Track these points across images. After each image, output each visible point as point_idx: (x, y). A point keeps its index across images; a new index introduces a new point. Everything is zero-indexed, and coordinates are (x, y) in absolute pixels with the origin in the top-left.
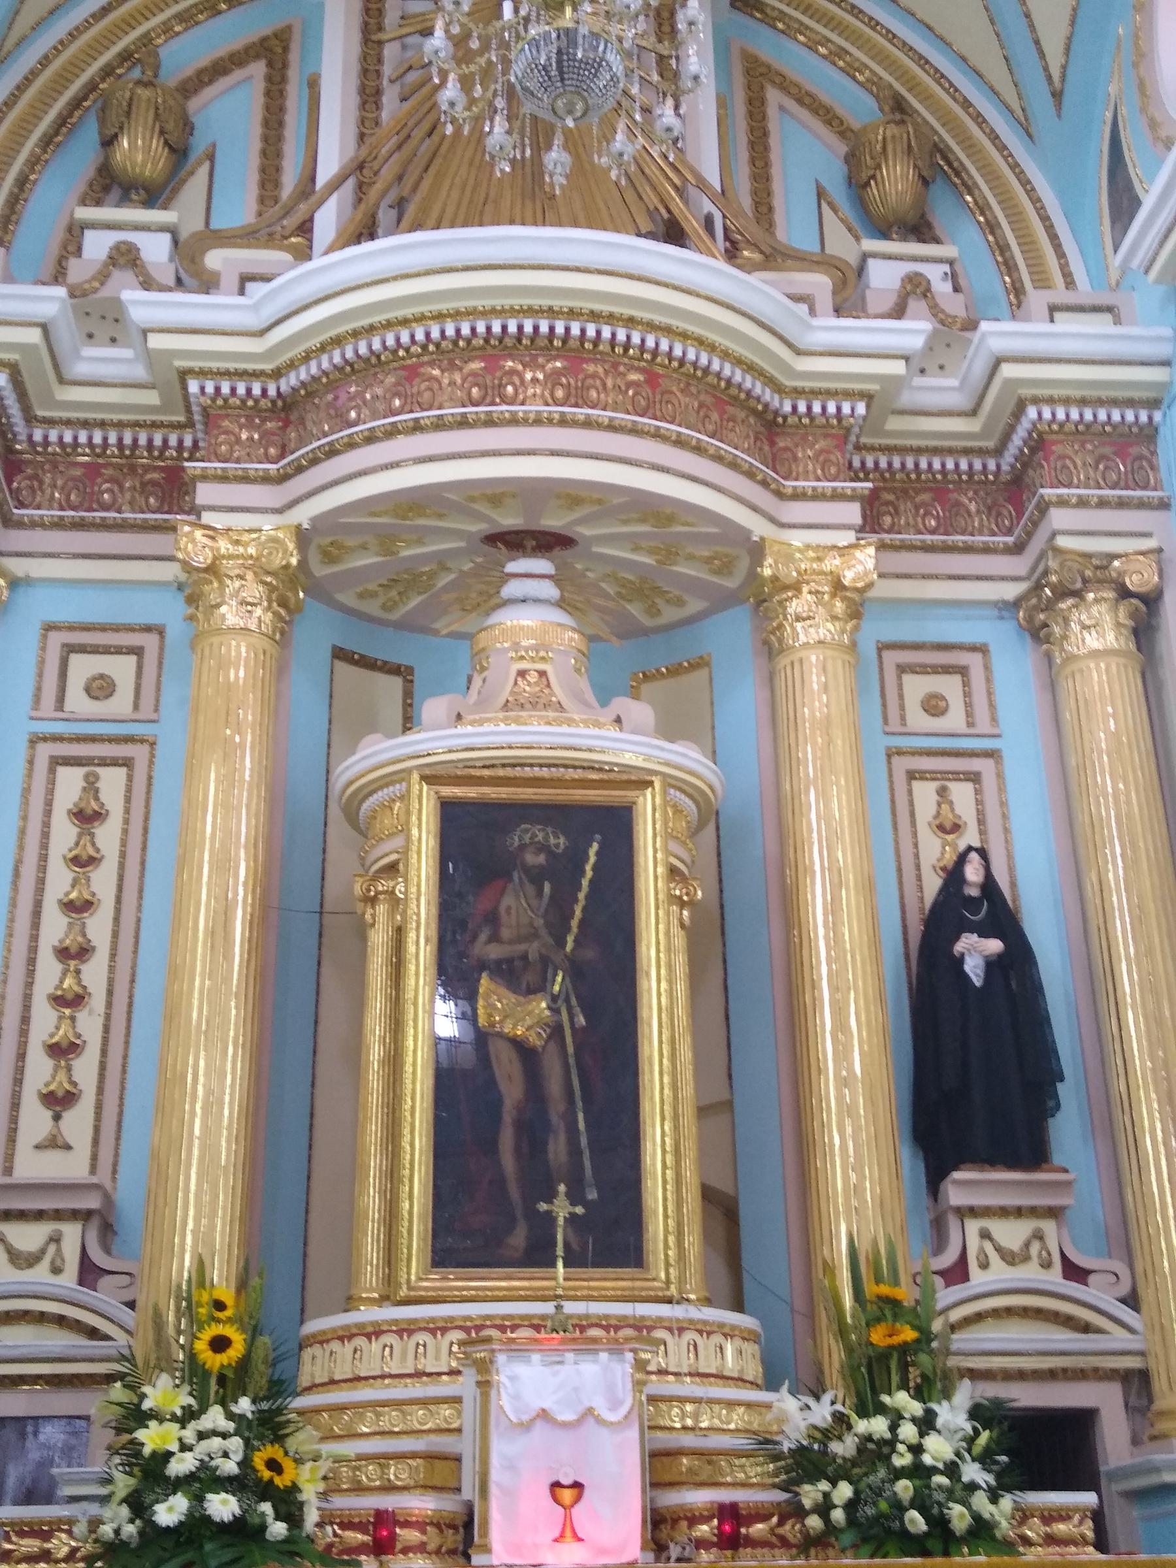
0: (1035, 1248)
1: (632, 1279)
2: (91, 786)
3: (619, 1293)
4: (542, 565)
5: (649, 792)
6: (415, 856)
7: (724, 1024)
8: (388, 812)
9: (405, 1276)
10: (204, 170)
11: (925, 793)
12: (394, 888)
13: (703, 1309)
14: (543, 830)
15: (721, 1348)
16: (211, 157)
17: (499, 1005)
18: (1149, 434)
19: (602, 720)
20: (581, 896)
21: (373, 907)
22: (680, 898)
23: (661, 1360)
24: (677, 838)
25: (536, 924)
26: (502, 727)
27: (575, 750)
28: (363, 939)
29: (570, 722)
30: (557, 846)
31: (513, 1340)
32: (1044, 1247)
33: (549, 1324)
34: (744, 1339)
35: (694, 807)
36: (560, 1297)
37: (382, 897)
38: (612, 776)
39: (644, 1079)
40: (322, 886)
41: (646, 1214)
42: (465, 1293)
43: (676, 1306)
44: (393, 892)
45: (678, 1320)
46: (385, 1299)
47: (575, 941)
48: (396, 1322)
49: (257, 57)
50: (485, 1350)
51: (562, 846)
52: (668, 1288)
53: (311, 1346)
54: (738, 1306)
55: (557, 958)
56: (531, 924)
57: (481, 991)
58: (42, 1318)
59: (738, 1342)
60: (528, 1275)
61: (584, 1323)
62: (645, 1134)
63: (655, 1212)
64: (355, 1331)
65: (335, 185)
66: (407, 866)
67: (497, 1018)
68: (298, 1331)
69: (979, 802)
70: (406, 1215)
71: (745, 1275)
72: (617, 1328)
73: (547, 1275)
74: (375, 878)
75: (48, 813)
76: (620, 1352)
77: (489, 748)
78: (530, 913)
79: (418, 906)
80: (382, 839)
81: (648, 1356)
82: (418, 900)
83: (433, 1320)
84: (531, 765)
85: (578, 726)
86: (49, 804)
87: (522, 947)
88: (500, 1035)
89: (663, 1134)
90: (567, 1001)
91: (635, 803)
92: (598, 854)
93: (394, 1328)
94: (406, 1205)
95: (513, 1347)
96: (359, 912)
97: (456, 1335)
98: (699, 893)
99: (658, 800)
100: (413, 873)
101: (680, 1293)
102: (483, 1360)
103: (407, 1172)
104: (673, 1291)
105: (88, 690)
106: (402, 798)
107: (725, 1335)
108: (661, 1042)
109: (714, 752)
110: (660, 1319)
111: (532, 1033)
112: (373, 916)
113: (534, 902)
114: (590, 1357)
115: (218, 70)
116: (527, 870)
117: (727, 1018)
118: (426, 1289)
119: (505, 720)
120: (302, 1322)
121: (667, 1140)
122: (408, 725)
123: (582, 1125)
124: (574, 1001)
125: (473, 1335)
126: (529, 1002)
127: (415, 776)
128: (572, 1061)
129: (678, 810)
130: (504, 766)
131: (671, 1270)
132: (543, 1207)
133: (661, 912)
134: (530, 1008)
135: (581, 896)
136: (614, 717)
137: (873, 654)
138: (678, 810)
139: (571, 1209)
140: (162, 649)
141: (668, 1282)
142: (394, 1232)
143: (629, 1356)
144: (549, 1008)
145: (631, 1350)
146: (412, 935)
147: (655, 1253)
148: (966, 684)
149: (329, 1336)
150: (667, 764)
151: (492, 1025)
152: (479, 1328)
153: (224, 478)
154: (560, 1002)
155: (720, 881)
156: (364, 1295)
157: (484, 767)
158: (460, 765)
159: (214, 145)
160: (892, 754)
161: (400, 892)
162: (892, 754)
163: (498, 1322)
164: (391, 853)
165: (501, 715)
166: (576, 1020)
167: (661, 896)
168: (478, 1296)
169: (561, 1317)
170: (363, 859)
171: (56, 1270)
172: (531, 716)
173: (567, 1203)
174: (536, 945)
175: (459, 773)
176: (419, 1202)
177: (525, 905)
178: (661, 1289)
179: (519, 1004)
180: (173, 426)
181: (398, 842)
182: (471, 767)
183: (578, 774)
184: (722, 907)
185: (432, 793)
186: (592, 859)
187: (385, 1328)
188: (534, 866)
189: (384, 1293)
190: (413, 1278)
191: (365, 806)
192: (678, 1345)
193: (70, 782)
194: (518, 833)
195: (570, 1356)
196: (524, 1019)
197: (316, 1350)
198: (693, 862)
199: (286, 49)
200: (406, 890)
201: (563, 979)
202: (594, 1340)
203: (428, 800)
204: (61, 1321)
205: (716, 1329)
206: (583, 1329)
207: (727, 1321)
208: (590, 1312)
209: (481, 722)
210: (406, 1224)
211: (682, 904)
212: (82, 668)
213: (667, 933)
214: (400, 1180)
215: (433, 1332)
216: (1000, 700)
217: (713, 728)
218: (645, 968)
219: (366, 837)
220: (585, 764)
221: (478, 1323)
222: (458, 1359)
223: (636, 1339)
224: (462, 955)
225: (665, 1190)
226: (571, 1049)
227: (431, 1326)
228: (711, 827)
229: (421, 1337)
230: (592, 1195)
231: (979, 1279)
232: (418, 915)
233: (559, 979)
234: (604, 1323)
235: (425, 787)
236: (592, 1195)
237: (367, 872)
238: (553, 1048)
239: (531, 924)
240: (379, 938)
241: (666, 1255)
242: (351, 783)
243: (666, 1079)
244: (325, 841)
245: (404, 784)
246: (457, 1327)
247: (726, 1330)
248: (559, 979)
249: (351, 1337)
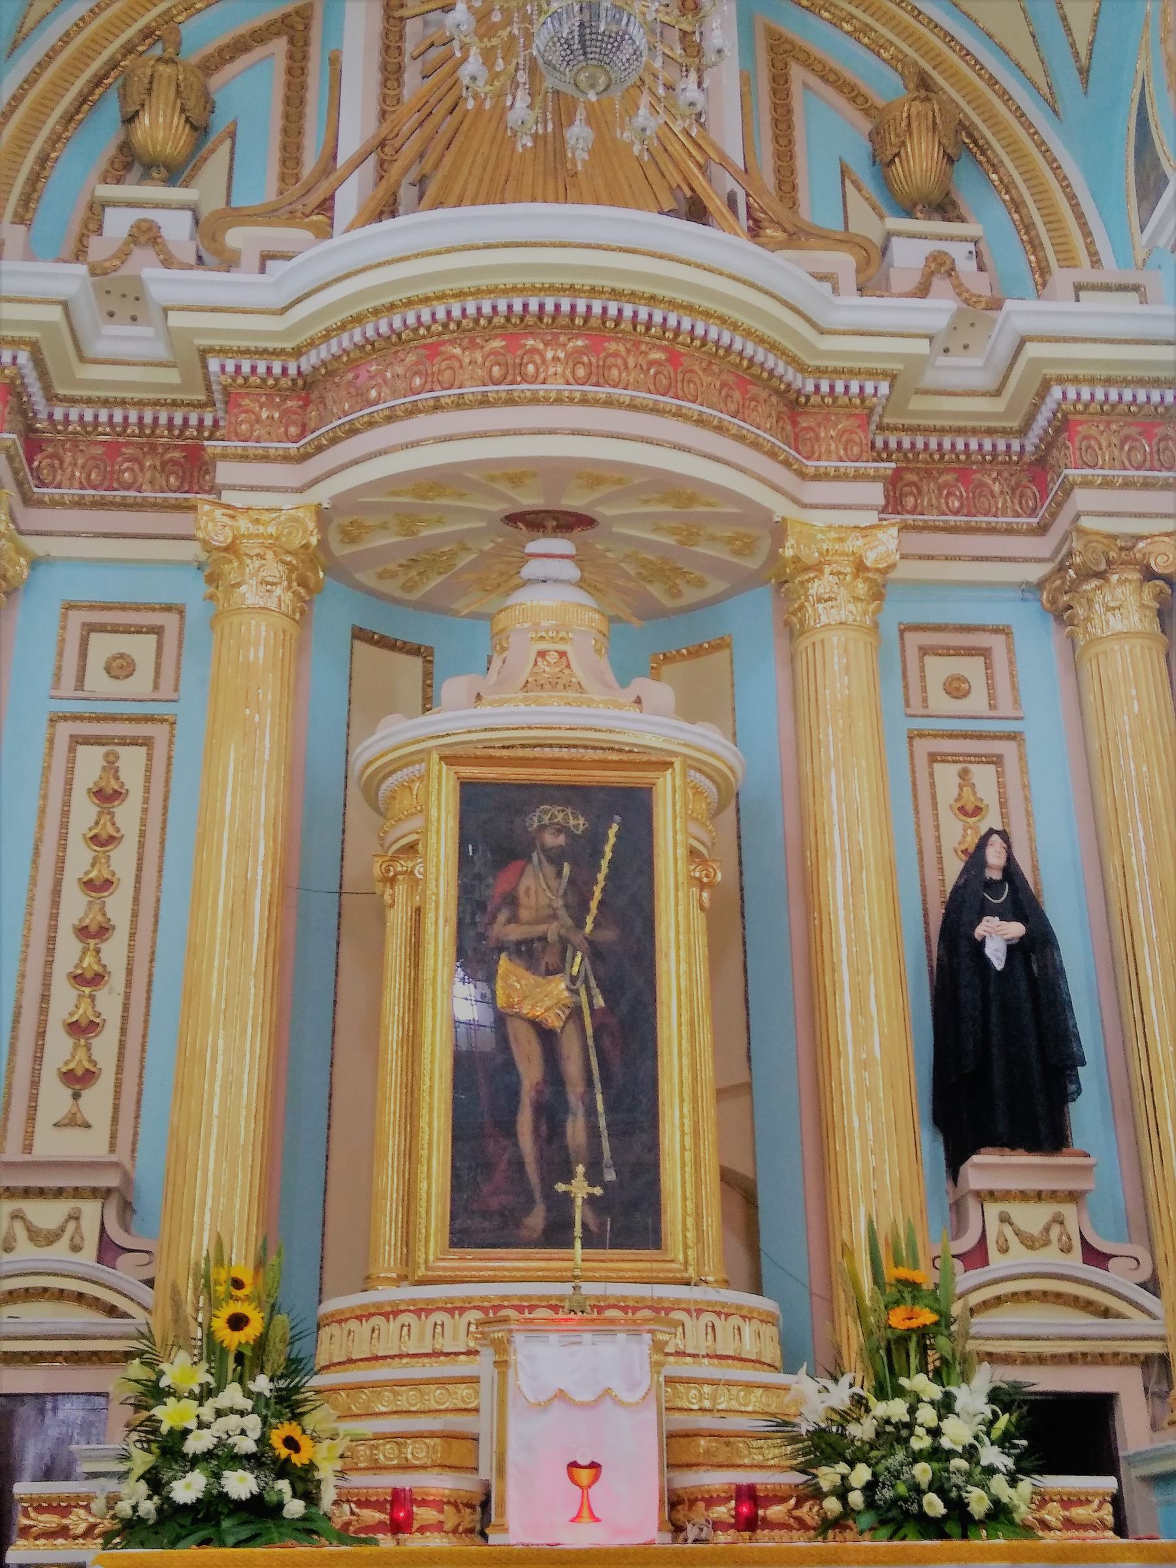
0: (1055, 1231)
16: (232, 135)
65: (358, 161)
75: (68, 792)
159: (235, 123)
171: (76, 1248)
193: (90, 761)
199: (307, 27)
212: (103, 647)
231: (998, 1263)
240: (398, 920)
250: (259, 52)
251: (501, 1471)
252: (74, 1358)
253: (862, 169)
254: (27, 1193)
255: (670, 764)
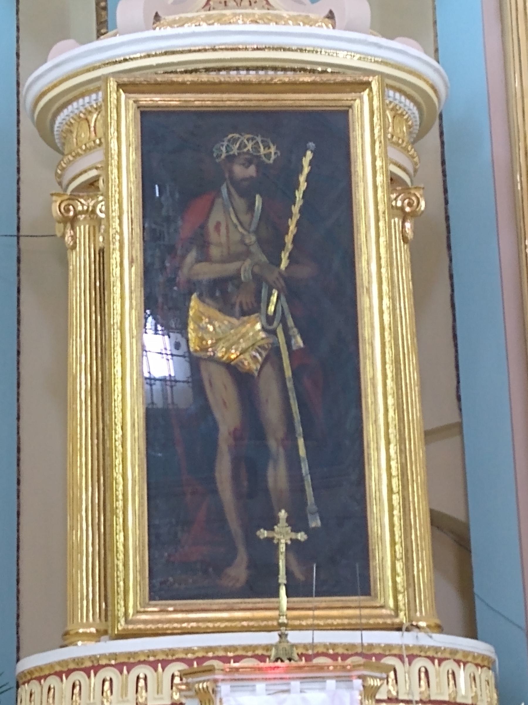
1: (360, 608)
3: (346, 621)
5: (365, 94)
6: (115, 171)
7: (452, 344)
8: (85, 125)
9: (123, 609)
12: (94, 207)
13: (435, 635)
14: (253, 139)
15: (453, 674)
17: (211, 328)
19: (312, 16)
20: (295, 209)
21: (73, 228)
22: (402, 209)
23: (391, 687)
24: (398, 144)
25: (247, 241)
26: (204, 27)
27: (285, 50)
28: (65, 263)
29: (278, 19)
30: (268, 156)
31: (237, 669)
33: (273, 653)
34: (477, 665)
35: (415, 110)
36: (285, 625)
37: (82, 217)
38: (325, 78)
39: (368, 400)
40: (18, 209)
41: (373, 540)
42: (185, 625)
43: (406, 634)
44: (93, 212)
45: (407, 647)
46: (101, 634)
47: (289, 257)
48: (115, 656)
50: (208, 680)
51: (273, 157)
52: (397, 615)
53: (28, 682)
54: (472, 634)
55: (272, 277)
56: (242, 242)
57: (191, 313)
59: (471, 668)
60: (250, 606)
61: (310, 652)
62: (369, 459)
63: (382, 538)
64: (72, 666)
66: (106, 182)
67: (210, 342)
68: (15, 669)
70: (121, 548)
71: (478, 602)
72: (345, 657)
73: (271, 605)
74: (73, 197)
76: (349, 679)
77: (190, 51)
78: (240, 229)
79: (121, 224)
80: (78, 154)
81: (378, 683)
82: (120, 218)
83: (153, 653)
84: (237, 69)
85: (286, 23)
87: (231, 268)
88: (213, 359)
89: (389, 459)
90: (283, 321)
91: (350, 107)
92: (311, 163)
93: (113, 662)
94: (121, 538)
95: (237, 676)
96: (59, 234)
97: (176, 668)
98: (423, 204)
99: (376, 103)
100: (113, 190)
101: (410, 620)
102: (206, 691)
103: (120, 504)
104: (402, 617)
106: (98, 109)
107: (458, 662)
108: (384, 363)
109: (436, 50)
110: (389, 647)
111: (247, 356)
112: (74, 238)
113: (245, 218)
114: (317, 685)
116: (235, 182)
117: (455, 337)
118: (145, 622)
119: (208, 20)
120: (18, 660)
121: (393, 464)
122: (103, 31)
123: (302, 452)
124: (290, 322)
125: (195, 665)
126: (243, 324)
127: (112, 84)
128: (290, 385)
129: (397, 114)
130: (207, 70)
131: (400, 597)
132: (263, 534)
133: (381, 224)
134: (244, 330)
135: (295, 209)
136: (326, 12)
138: (397, 114)
139: (293, 535)
141: (397, 608)
142: (109, 566)
143: (358, 683)
144: (263, 329)
145: (359, 677)
146: (116, 255)
147: (383, 580)
149: (47, 672)
150: (385, 63)
151: (205, 349)
152: (201, 660)
154: (275, 323)
155: (446, 191)
156: (81, 631)
157: (186, 72)
158: (160, 71)
161: (101, 211)
163: (221, 653)
164: (90, 169)
165: (203, 14)
166: (293, 342)
167: (381, 207)
168: (198, 627)
169: (285, 645)
170: (60, 176)
172: (235, 15)
173: (289, 529)
174: (248, 262)
175: (159, 79)
176: (134, 534)
177: (235, 220)
178: (390, 616)
179: (232, 327)
181: (96, 157)
182: (171, 72)
183: (288, 77)
184: (447, 218)
185: (131, 102)
186: (306, 170)
187: (103, 662)
188: (244, 179)
189: (102, 628)
190: (131, 611)
191: (59, 119)
192: (409, 673)
194: (225, 143)
195: (296, 684)
196: (237, 342)
197: (34, 686)
198: (415, 171)
200: (107, 208)
201: (278, 298)
202: (321, 668)
203: (127, 110)
205: (447, 655)
206: (309, 658)
207: (458, 647)
208: (316, 641)
209: (181, 23)
210: (121, 556)
211: (405, 217)
213: (389, 245)
214: (113, 512)
215: (154, 665)
217: (435, 23)
218: (366, 284)
219: (63, 154)
220: (296, 66)
221: (200, 654)
222: (180, 691)
223: (365, 666)
224: (172, 282)
225: (391, 516)
226: (288, 373)
227: (152, 659)
228: (435, 129)
229: (142, 671)
230: (315, 523)
232: (121, 234)
233: (274, 299)
234: (331, 652)
235: (123, 96)
236: (315, 523)
237: (65, 190)
238: (269, 370)
239: (242, 242)
241: (394, 582)
242: (43, 94)
243: (391, 401)
244: (19, 160)
245: (100, 94)
246: (178, 660)
247: (459, 657)
248: (274, 299)
249: (69, 673)
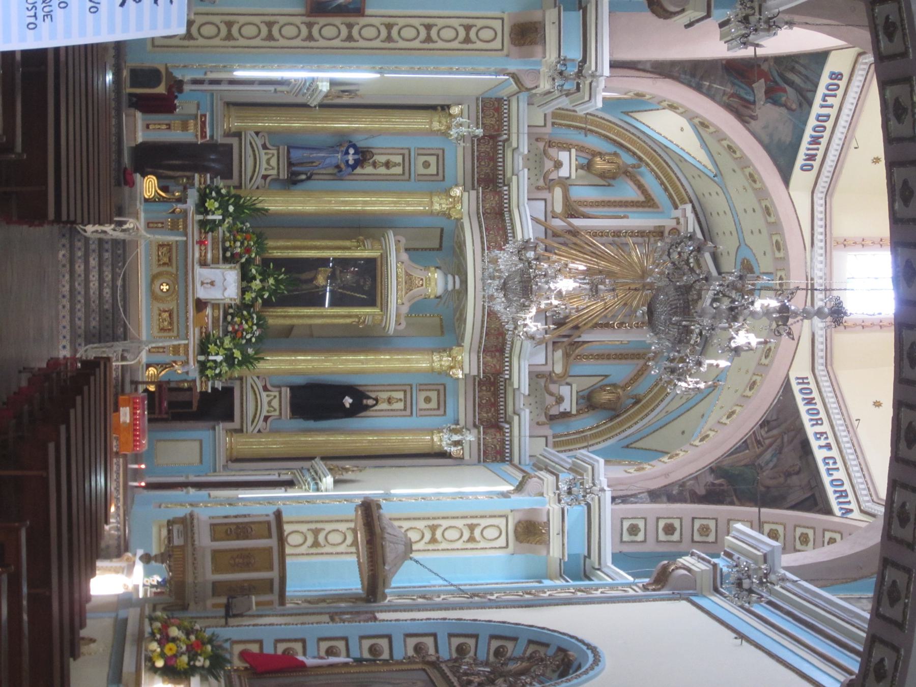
0: (272, 409)
2: (396, 165)
4: (458, 286)
10: (605, 183)
11: (400, 395)
16: (609, 185)
18: (503, 460)
32: (272, 411)
49: (646, 198)
58: (255, 167)
65: (570, 224)
69: (397, 410)
75: (388, 154)
86: (391, 154)
105: (426, 162)
115: (640, 187)
137: (443, 382)
140: (438, 181)
148: (434, 409)
153: (478, 198)
159: (613, 186)
160: (411, 385)
162: (411, 385)
171: (266, 169)
180: (504, 181)
193: (398, 159)
199: (650, 207)
204: (254, 171)
212: (432, 160)
216: (428, 418)
231: (264, 394)
240: (347, 243)
250: (639, 192)
251: (212, 268)
252: (240, 171)
253: (606, 381)
254: (278, 157)
255: (382, 311)
